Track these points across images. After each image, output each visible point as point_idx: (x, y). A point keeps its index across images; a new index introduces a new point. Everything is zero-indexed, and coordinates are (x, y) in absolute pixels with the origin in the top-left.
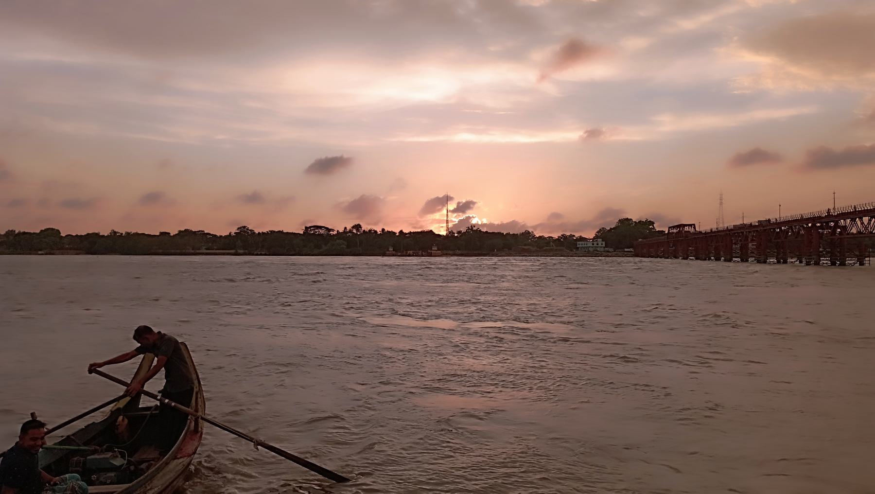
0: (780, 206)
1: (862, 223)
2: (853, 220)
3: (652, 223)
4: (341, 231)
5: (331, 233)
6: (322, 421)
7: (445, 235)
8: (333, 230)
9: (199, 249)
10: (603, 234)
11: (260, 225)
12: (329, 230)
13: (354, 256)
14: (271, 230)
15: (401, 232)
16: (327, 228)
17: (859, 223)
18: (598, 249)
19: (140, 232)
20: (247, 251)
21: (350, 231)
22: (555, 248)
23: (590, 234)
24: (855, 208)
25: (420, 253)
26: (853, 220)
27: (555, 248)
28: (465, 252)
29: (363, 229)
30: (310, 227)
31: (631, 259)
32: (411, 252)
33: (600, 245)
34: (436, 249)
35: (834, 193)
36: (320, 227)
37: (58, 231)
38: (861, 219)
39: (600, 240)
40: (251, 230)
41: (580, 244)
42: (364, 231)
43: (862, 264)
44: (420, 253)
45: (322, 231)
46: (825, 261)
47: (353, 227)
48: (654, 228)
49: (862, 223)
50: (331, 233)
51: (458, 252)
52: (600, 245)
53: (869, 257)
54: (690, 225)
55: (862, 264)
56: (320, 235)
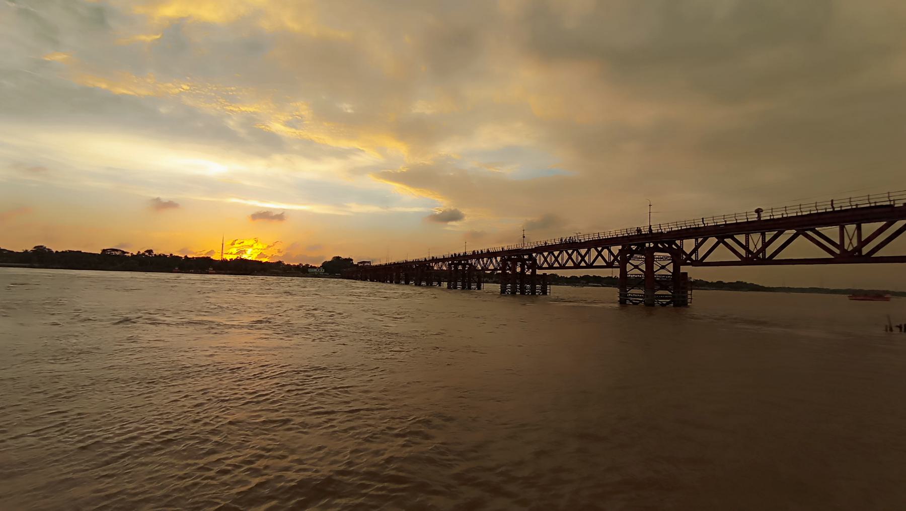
1: (496, 261)
3: (352, 260)
4: (135, 254)
5: (126, 254)
7: (100, 253)
8: (128, 253)
10: (326, 265)
11: (57, 247)
13: (884, 246)
17: (481, 262)
18: (320, 273)
19: (771, 287)
21: (143, 254)
22: (294, 271)
23: (319, 265)
24: (546, 243)
27: (294, 271)
28: (231, 272)
29: (154, 253)
35: (650, 205)
36: (117, 250)
37: (280, 262)
38: (496, 258)
39: (322, 268)
40: (48, 249)
41: (310, 270)
42: (155, 255)
43: (440, 285)
47: (146, 251)
48: (352, 263)
49: (496, 261)
50: (126, 254)
51: (228, 272)
54: (368, 262)
55: (440, 285)
56: (116, 255)
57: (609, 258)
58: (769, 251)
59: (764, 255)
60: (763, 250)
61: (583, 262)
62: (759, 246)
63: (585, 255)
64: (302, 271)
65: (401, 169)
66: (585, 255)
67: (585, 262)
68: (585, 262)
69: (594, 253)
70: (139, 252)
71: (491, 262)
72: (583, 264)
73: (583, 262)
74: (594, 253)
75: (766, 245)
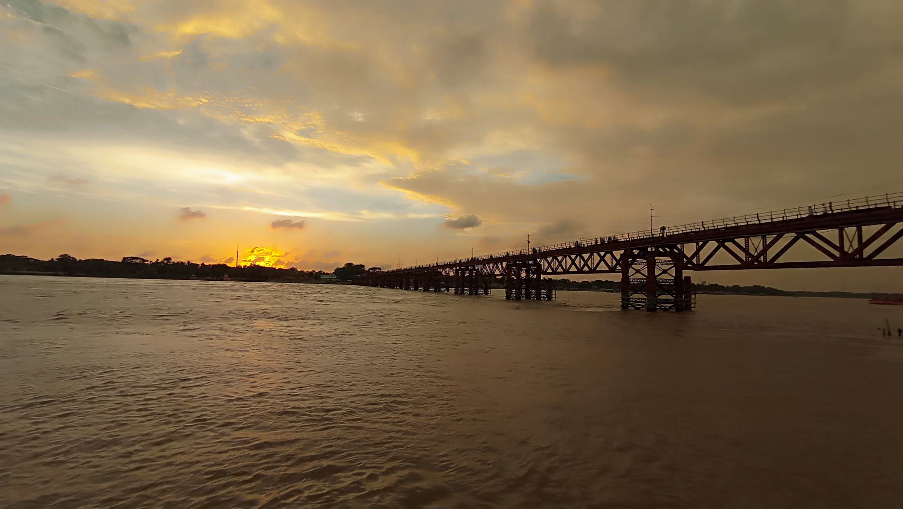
0: (529, 242)
2: (484, 265)
3: (363, 266)
5: (146, 262)
6: (175, 456)
8: (148, 261)
9: (20, 270)
10: (338, 271)
12: (145, 261)
14: (92, 258)
15: (203, 264)
16: (143, 259)
20: (67, 273)
21: (162, 262)
25: (215, 278)
26: (484, 265)
29: (172, 261)
30: (128, 258)
31: (350, 286)
32: (208, 278)
33: (333, 277)
34: (227, 276)
36: (137, 258)
41: (322, 277)
42: (173, 262)
44: (215, 278)
45: (138, 261)
46: (432, 289)
47: (165, 259)
52: (333, 277)
53: (491, 288)
54: (379, 268)
57: (580, 263)
58: (771, 253)
59: (765, 258)
60: (764, 252)
61: (586, 266)
62: (761, 248)
63: (588, 259)
64: (315, 277)
65: (411, 175)
66: (588, 259)
67: (589, 267)
68: (589, 267)
69: (597, 258)
70: (157, 260)
71: (497, 267)
72: (586, 269)
73: (586, 266)
74: (597, 258)
75: (766, 247)
